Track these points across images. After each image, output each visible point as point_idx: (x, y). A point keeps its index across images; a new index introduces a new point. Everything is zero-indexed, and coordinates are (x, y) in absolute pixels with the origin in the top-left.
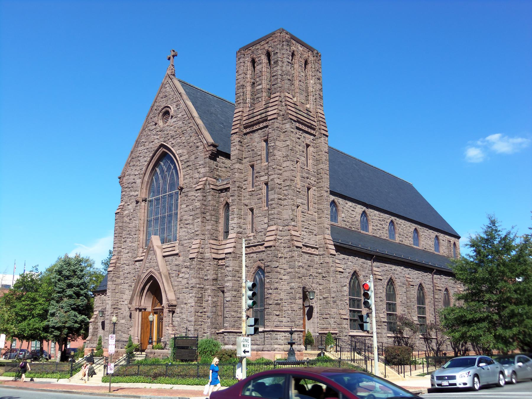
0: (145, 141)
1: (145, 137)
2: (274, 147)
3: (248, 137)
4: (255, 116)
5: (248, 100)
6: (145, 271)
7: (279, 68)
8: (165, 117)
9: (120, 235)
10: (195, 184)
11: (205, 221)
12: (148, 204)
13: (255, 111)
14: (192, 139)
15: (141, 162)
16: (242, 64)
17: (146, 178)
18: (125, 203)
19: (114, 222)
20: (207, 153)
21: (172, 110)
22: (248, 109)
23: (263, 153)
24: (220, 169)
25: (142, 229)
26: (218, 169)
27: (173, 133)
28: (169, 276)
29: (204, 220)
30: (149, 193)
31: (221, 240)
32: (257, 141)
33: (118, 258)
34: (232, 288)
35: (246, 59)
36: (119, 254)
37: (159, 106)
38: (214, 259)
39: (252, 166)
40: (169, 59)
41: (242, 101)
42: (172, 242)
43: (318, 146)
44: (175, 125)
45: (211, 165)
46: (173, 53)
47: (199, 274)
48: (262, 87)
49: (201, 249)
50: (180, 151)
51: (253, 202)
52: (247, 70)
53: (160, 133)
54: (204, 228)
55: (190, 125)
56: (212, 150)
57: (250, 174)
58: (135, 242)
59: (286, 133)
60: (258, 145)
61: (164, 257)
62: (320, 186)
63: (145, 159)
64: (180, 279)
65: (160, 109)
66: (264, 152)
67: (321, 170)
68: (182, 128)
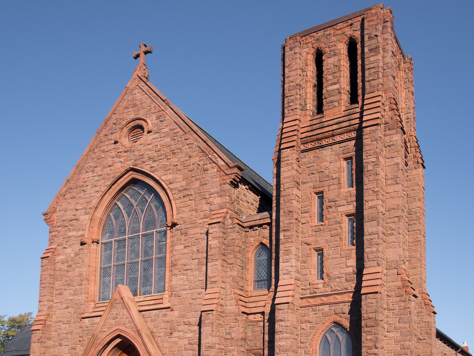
0: (95, 165)
1: (95, 160)
2: (376, 163)
3: (311, 155)
4: (325, 126)
5: (308, 105)
6: (106, 330)
7: (380, 57)
8: (132, 134)
9: (51, 285)
10: (201, 219)
11: (225, 264)
12: (101, 247)
13: (324, 120)
14: (193, 160)
15: (87, 193)
16: (298, 56)
17: (99, 213)
18: (58, 246)
19: (39, 269)
20: (226, 177)
21: (150, 123)
22: (309, 118)
23: (342, 175)
24: (241, 202)
25: (92, 278)
26: (239, 202)
27: (151, 153)
28: (153, 336)
29: (224, 263)
30: (102, 234)
31: (249, 290)
32: (328, 159)
33: (48, 315)
34: (290, 347)
35: (304, 50)
36: (51, 310)
37: (122, 119)
38: (243, 312)
39: (320, 195)
40: (137, 56)
41: (298, 106)
42: (153, 295)
43: (411, 180)
44: (157, 143)
45: (232, 194)
46: (144, 49)
47: (219, 331)
48: (341, 86)
49: (221, 301)
50: (170, 177)
51: (322, 239)
52: (307, 65)
53: (126, 154)
54: (224, 274)
55: (188, 142)
56: (236, 173)
57: (314, 204)
58: (81, 294)
59: (392, 147)
60: (332, 166)
61: (141, 311)
62: (416, 229)
63: (97, 189)
64: (176, 339)
65: (124, 123)
66: (344, 175)
67: (418, 209)
68: (171, 147)
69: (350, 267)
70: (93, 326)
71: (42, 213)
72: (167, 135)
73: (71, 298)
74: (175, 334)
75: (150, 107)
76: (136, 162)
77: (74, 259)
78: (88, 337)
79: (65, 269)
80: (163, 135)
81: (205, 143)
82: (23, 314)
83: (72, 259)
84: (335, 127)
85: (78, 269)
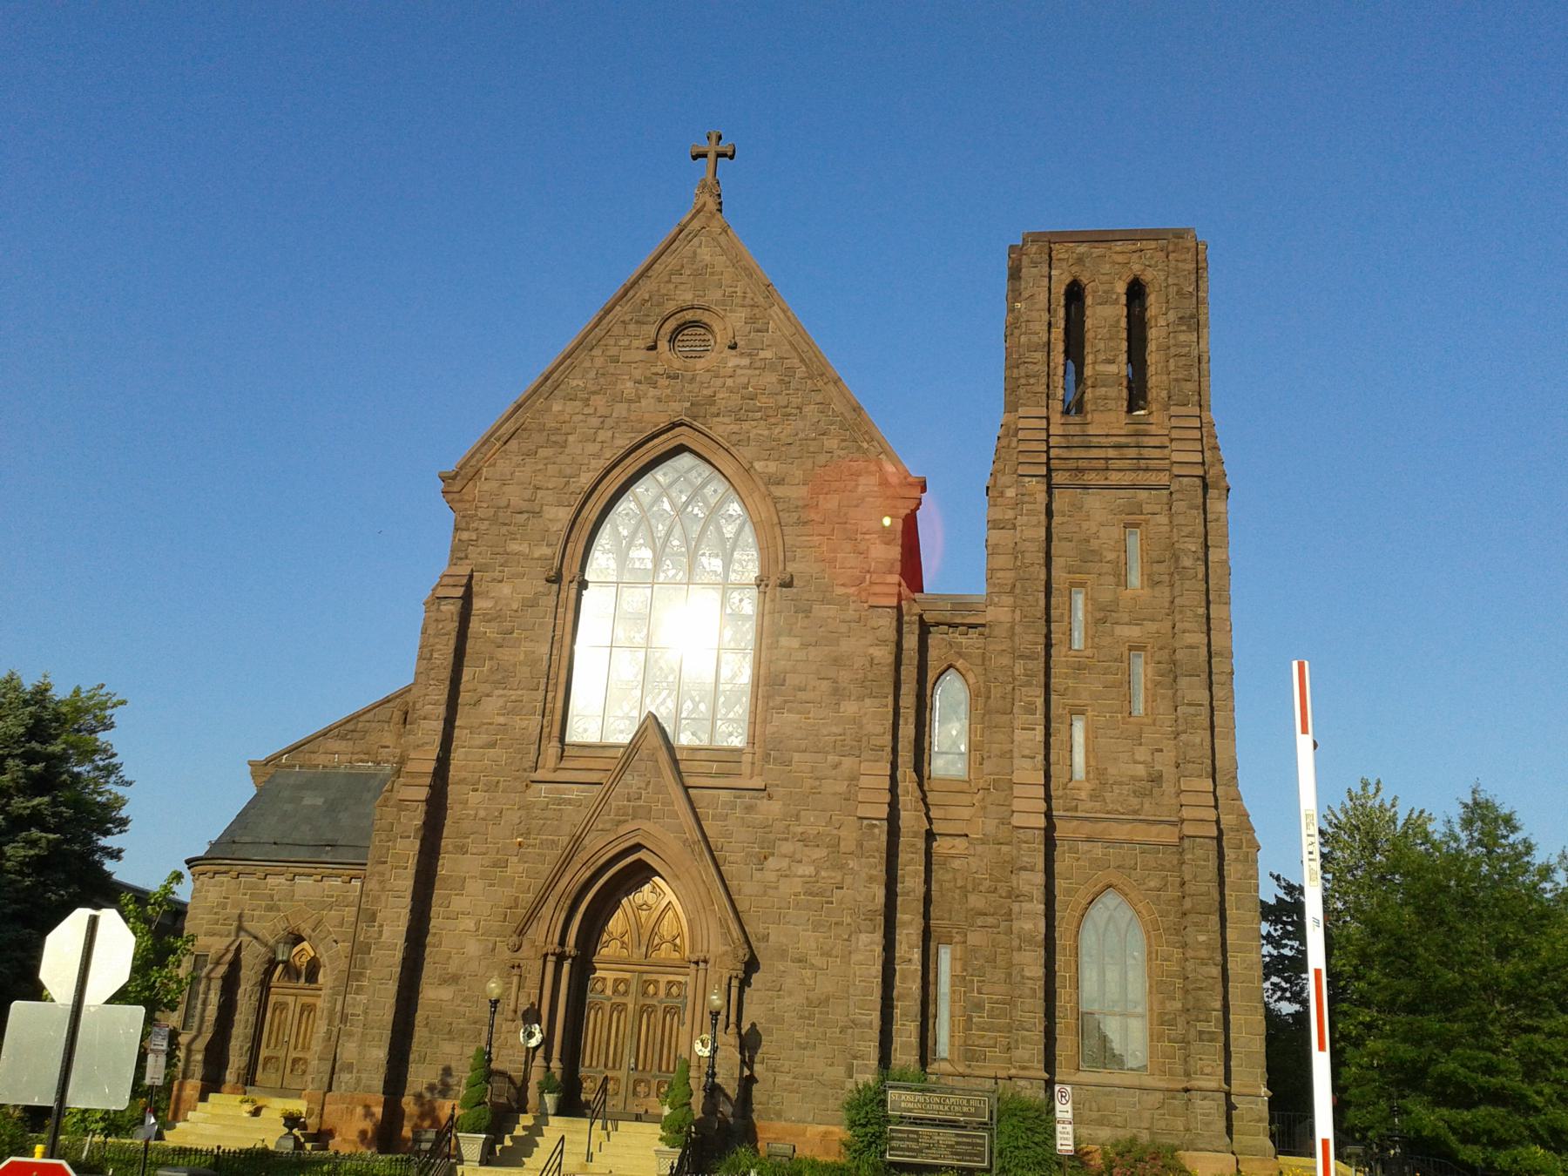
69: (1140, 763)
70: (560, 810)
71: (440, 473)
72: (767, 366)
73: (502, 720)
74: (772, 863)
75: (733, 289)
76: (695, 410)
77: (517, 614)
78: (544, 837)
79: (492, 635)
80: (758, 364)
81: (1045, 748)
82: (61, 692)
83: (513, 614)
84: (1111, 453)
85: (526, 644)
